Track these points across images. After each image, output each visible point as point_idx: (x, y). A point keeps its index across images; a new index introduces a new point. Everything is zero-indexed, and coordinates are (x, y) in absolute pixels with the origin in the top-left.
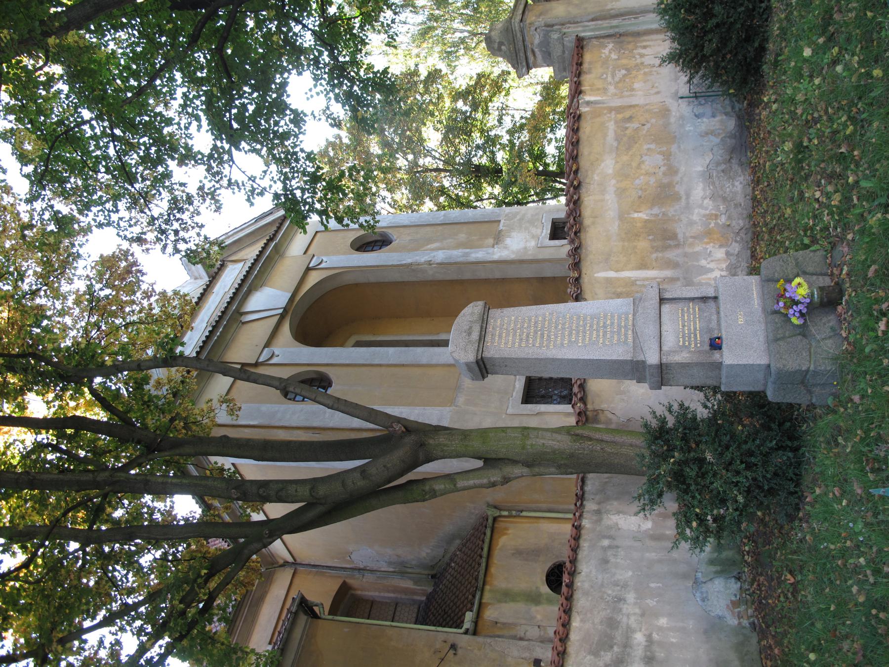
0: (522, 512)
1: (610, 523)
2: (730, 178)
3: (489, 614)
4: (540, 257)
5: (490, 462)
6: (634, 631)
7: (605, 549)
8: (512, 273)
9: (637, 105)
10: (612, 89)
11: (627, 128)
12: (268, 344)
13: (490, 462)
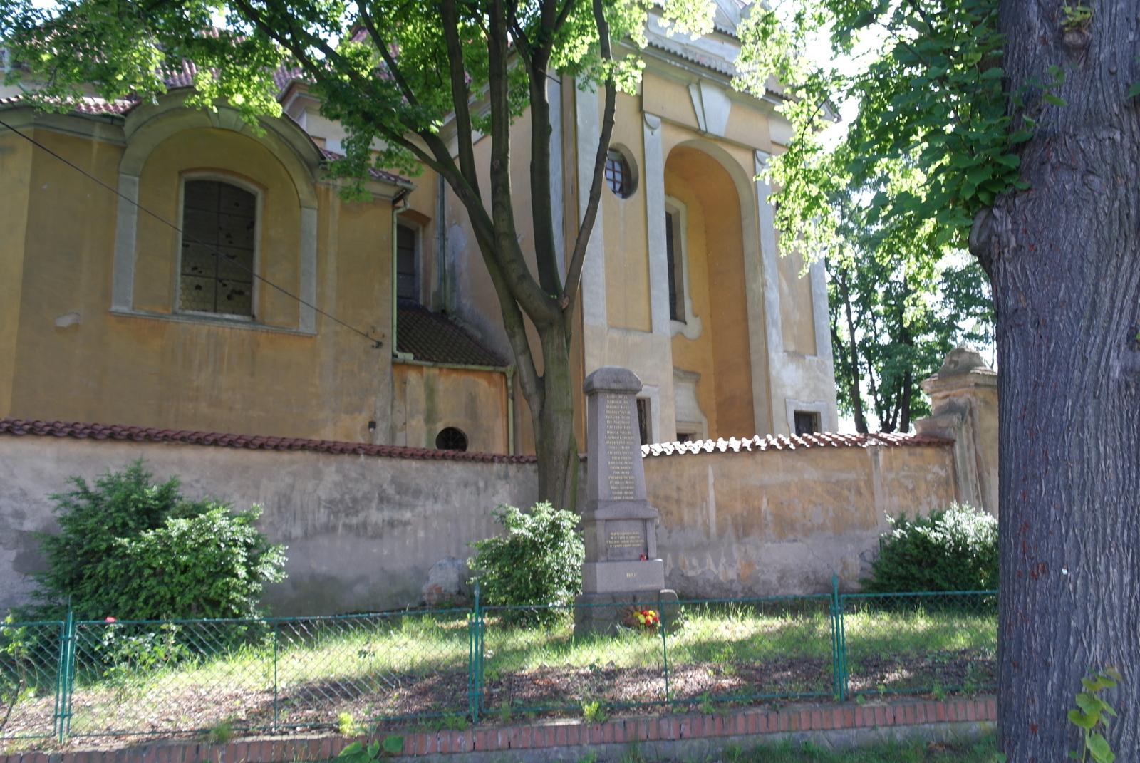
0: (513, 399)
1: (499, 487)
2: (802, 583)
3: (413, 376)
4: (774, 402)
5: (541, 383)
6: (412, 511)
7: (476, 484)
8: (757, 372)
9: (874, 500)
10: (892, 476)
11: (850, 490)
12: (665, 121)
13: (541, 383)
